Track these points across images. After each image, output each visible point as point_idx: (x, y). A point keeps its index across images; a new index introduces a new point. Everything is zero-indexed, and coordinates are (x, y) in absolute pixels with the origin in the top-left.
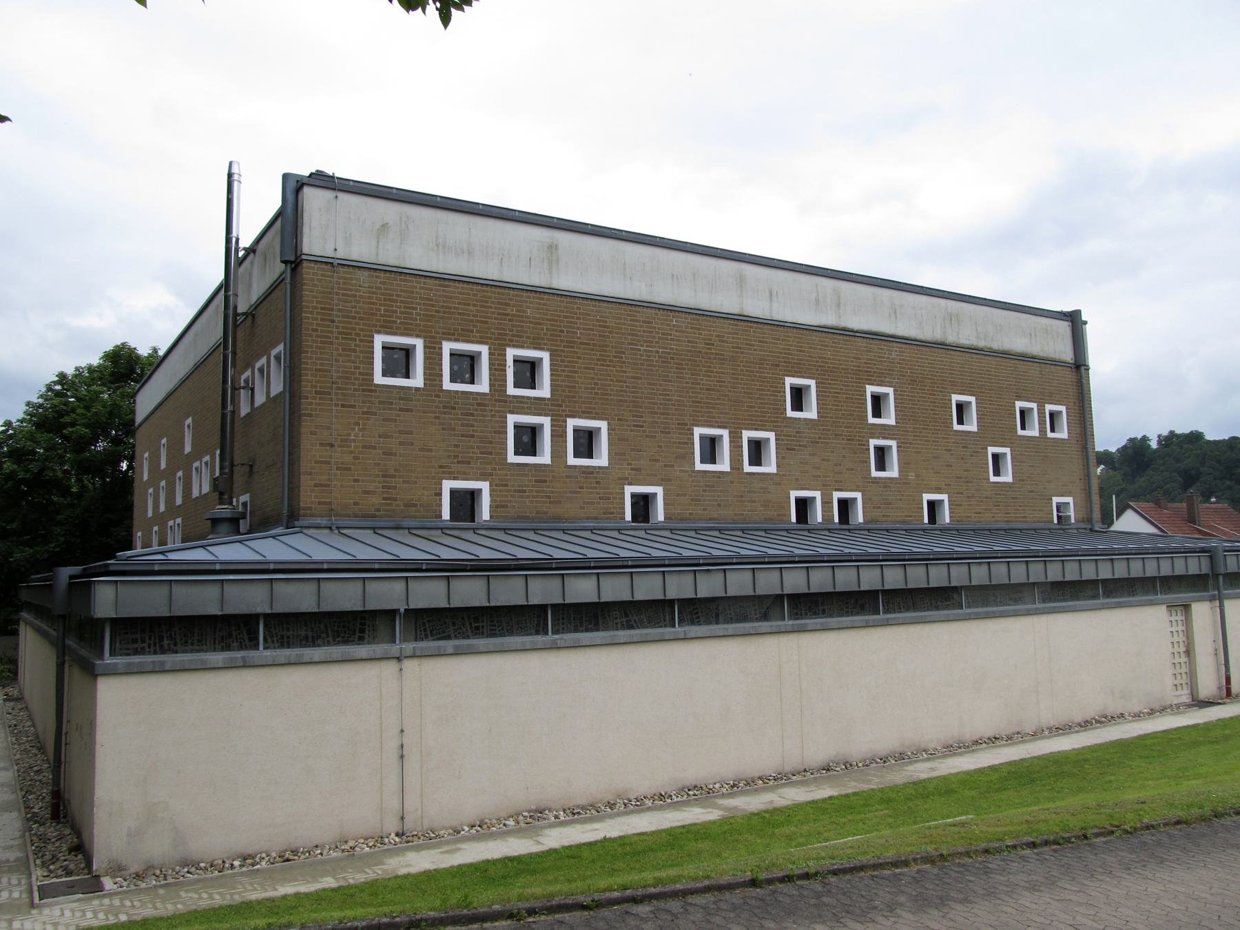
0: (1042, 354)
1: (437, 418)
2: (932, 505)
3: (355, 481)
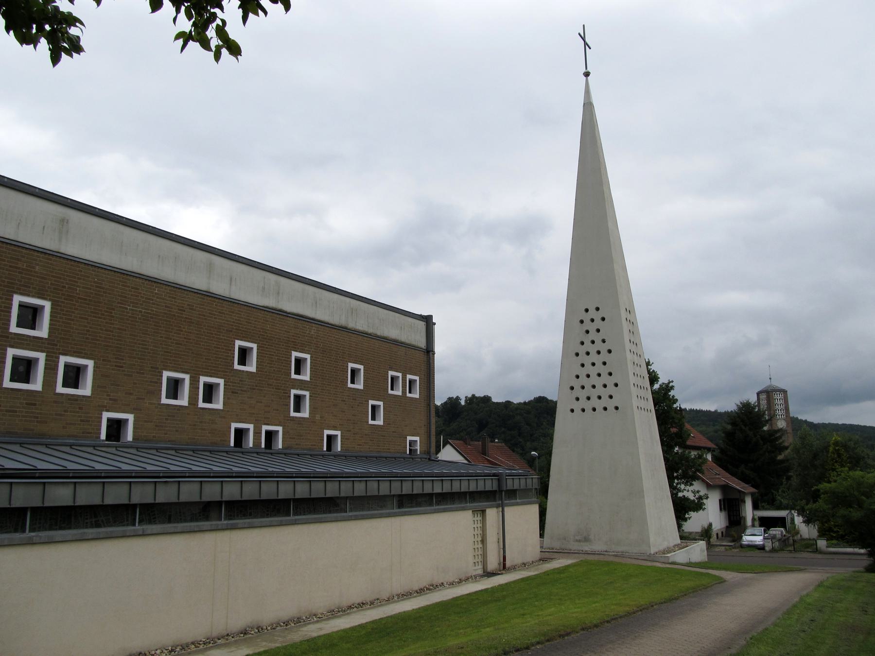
2: (330, 438)
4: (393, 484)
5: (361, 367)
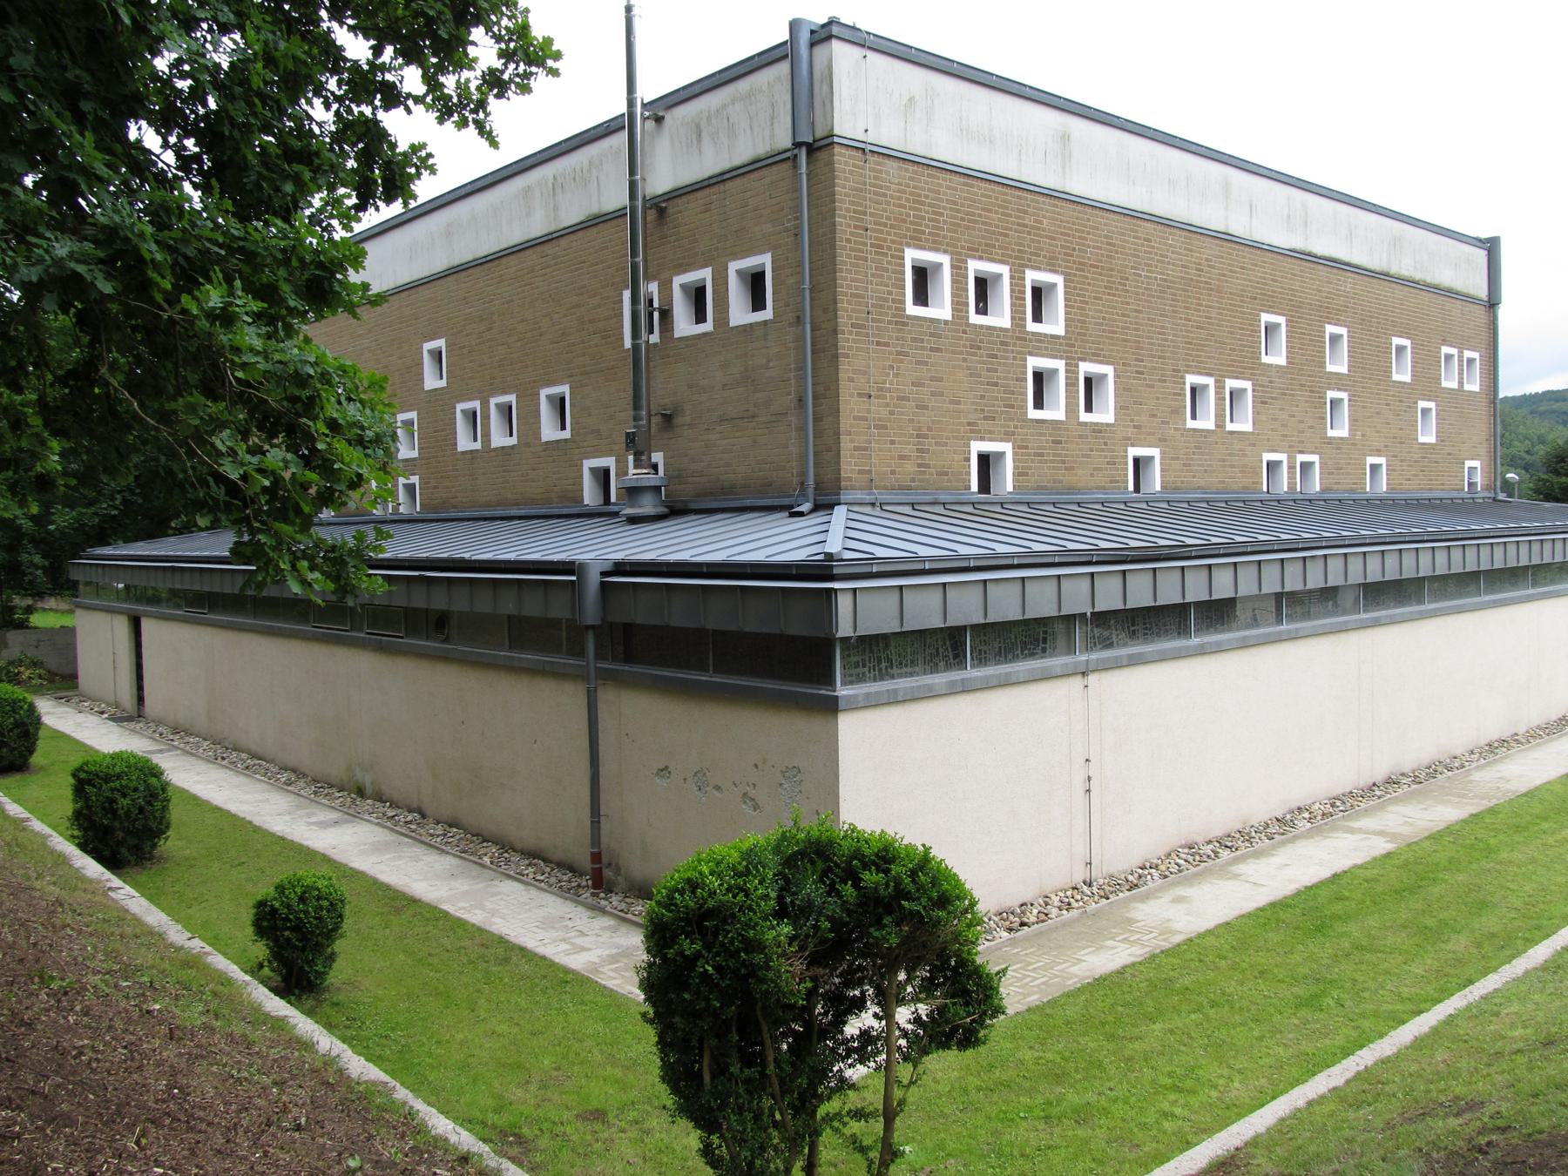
0: (1465, 291)
1: (965, 360)
2: (985, 460)
3: (892, 442)
4: (1289, 568)
5: (1058, 280)
